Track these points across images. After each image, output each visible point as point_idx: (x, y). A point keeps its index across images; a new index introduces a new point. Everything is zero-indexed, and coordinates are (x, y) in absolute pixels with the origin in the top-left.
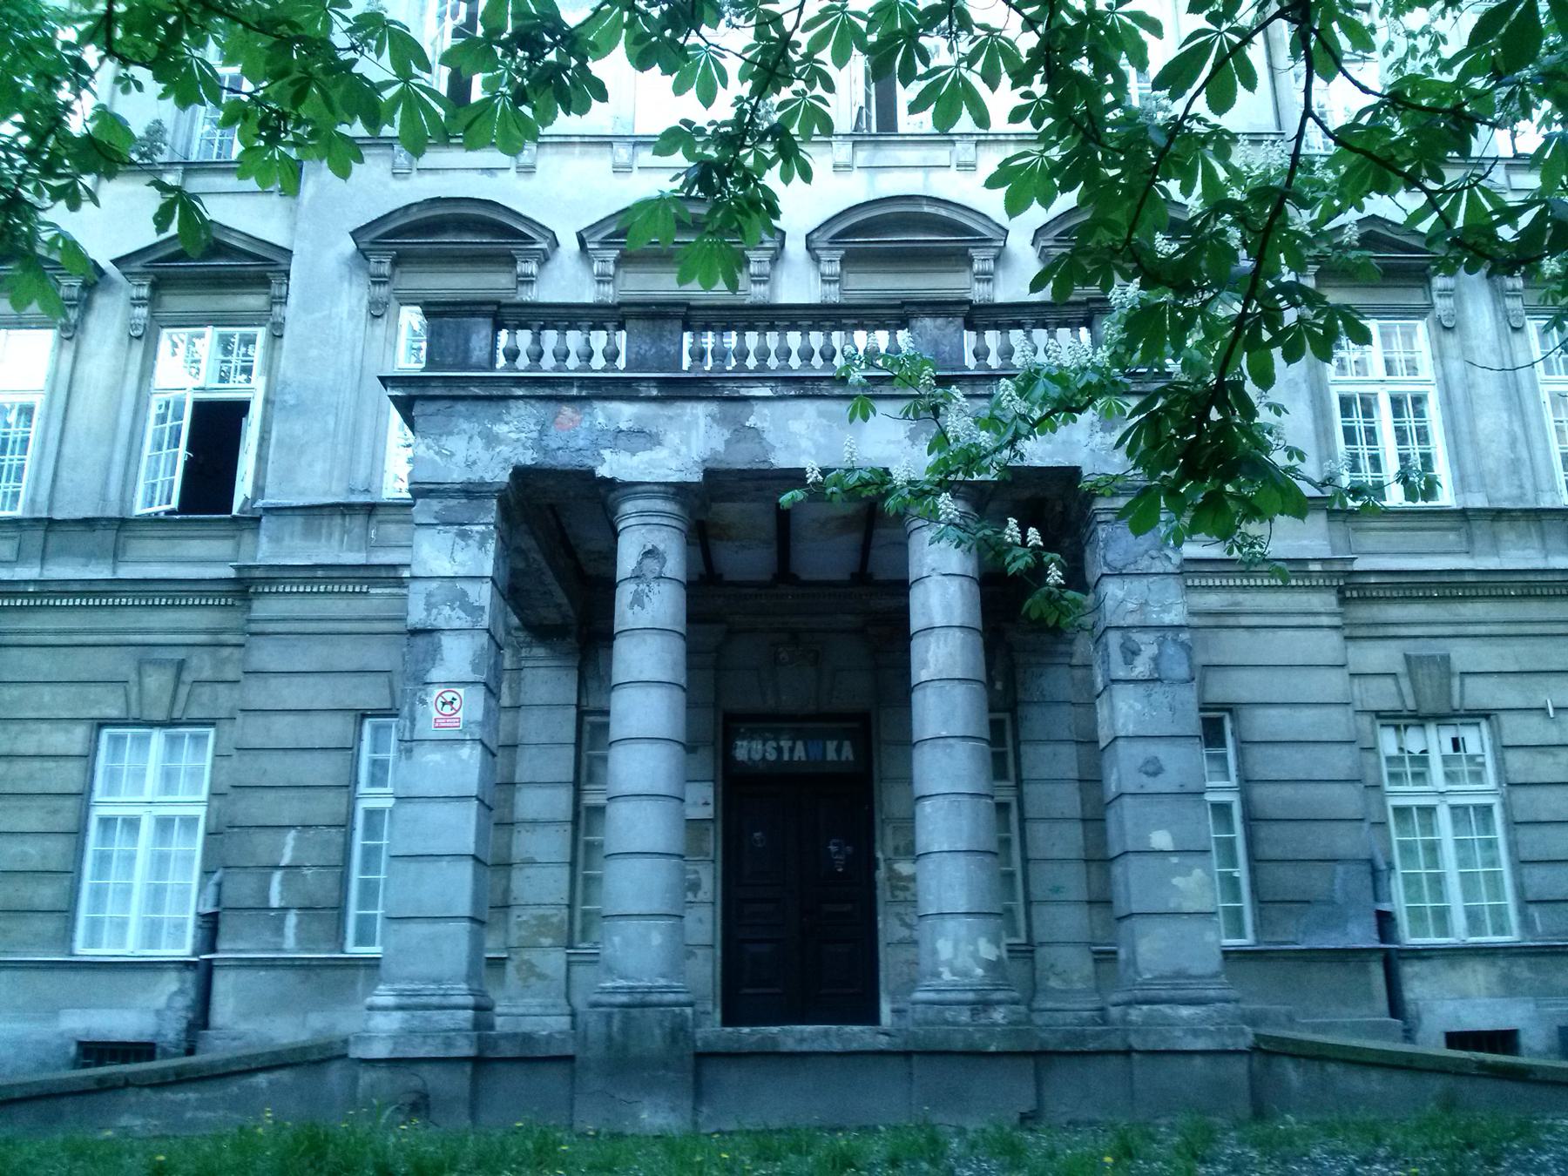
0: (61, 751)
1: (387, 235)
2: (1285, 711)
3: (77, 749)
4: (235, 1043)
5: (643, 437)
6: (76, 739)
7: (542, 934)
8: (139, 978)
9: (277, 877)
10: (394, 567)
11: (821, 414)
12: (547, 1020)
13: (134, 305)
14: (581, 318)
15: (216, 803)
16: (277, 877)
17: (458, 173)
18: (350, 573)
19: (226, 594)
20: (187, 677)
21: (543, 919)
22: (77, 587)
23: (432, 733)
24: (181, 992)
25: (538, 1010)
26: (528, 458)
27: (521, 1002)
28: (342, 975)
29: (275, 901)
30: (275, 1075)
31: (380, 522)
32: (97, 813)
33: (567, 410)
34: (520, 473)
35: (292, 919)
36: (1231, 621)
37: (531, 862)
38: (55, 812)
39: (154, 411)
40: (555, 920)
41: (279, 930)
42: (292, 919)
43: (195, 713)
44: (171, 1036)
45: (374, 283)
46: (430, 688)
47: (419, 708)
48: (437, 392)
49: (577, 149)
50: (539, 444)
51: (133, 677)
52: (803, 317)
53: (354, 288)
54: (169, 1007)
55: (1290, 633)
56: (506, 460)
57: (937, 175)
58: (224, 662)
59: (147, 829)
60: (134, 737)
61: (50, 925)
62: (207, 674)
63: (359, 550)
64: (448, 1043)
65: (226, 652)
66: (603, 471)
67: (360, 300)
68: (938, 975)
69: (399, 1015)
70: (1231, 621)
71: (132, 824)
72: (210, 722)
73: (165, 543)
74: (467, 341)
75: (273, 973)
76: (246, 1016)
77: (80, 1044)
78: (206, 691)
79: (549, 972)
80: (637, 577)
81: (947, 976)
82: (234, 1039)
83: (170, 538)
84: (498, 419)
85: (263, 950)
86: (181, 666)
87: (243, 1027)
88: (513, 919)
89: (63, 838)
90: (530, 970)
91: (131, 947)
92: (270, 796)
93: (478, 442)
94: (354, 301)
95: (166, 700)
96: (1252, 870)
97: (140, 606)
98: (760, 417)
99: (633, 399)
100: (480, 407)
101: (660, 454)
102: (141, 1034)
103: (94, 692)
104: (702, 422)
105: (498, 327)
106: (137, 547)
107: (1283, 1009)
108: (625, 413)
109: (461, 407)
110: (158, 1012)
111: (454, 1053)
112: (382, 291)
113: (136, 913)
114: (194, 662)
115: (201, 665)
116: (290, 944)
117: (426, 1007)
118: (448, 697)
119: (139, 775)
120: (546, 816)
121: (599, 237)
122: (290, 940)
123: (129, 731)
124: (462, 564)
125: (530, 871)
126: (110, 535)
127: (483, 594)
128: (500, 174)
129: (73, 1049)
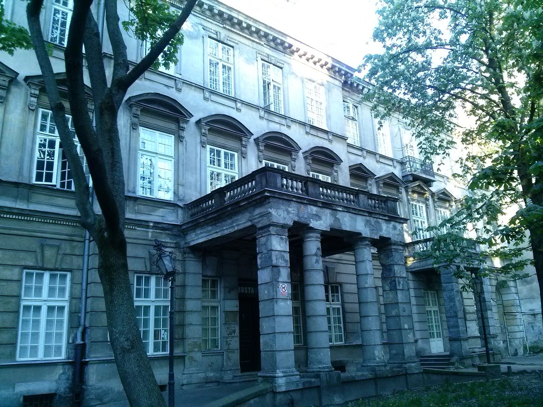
0: (9, 278)
1: (141, 101)
2: (350, 285)
3: (16, 278)
4: (99, 391)
5: (318, 217)
6: (14, 273)
7: (195, 348)
8: (46, 369)
10: (147, 222)
11: (350, 217)
12: (199, 374)
13: (32, 96)
14: (298, 178)
15: (74, 301)
17: (157, 84)
18: (133, 222)
20: (61, 252)
21: (195, 343)
22: (16, 211)
23: (281, 297)
24: (64, 373)
25: (196, 372)
26: (296, 219)
27: (190, 369)
30: (255, 399)
31: (138, 204)
32: (23, 303)
33: (302, 206)
34: (295, 222)
36: (340, 261)
37: (191, 324)
38: (8, 303)
39: (38, 142)
40: (198, 343)
43: (64, 266)
44: (62, 390)
45: (134, 116)
46: (279, 283)
47: (278, 289)
48: (277, 196)
49: (193, 88)
51: (38, 250)
52: (340, 189)
53: (125, 116)
54: (59, 379)
55: (350, 266)
56: (292, 219)
57: (282, 127)
58: (74, 247)
59: (44, 310)
60: (60, 275)
62: (68, 251)
63: (132, 213)
64: (297, 385)
65: (75, 243)
66: (311, 225)
67: (127, 121)
68: (376, 359)
69: (284, 378)
70: (340, 261)
71: (38, 309)
72: (70, 270)
73: (47, 197)
74: (276, 180)
75: (109, 365)
76: (100, 381)
78: (68, 258)
79: (198, 359)
81: (377, 359)
82: (98, 389)
83: (51, 196)
84: (289, 207)
85: (107, 357)
86: (59, 247)
87: (100, 385)
88: (187, 343)
89: (12, 314)
90: (192, 358)
93: (286, 212)
94: (126, 121)
95: (53, 261)
96: (344, 325)
97: (41, 222)
98: (340, 215)
100: (285, 202)
101: (321, 222)
102: (50, 390)
103: (22, 255)
104: (329, 215)
105: (282, 178)
106: (37, 197)
107: (351, 359)
109: (281, 201)
110: (56, 381)
111: (299, 388)
112: (136, 120)
113: (41, 343)
114: (63, 246)
115: (66, 248)
117: (290, 376)
118: (284, 286)
119: (39, 290)
120: (195, 309)
121: (205, 121)
123: (35, 271)
124: (282, 247)
125: (191, 327)
126: (25, 191)
127: (287, 256)
128: (171, 88)
129: (22, 399)
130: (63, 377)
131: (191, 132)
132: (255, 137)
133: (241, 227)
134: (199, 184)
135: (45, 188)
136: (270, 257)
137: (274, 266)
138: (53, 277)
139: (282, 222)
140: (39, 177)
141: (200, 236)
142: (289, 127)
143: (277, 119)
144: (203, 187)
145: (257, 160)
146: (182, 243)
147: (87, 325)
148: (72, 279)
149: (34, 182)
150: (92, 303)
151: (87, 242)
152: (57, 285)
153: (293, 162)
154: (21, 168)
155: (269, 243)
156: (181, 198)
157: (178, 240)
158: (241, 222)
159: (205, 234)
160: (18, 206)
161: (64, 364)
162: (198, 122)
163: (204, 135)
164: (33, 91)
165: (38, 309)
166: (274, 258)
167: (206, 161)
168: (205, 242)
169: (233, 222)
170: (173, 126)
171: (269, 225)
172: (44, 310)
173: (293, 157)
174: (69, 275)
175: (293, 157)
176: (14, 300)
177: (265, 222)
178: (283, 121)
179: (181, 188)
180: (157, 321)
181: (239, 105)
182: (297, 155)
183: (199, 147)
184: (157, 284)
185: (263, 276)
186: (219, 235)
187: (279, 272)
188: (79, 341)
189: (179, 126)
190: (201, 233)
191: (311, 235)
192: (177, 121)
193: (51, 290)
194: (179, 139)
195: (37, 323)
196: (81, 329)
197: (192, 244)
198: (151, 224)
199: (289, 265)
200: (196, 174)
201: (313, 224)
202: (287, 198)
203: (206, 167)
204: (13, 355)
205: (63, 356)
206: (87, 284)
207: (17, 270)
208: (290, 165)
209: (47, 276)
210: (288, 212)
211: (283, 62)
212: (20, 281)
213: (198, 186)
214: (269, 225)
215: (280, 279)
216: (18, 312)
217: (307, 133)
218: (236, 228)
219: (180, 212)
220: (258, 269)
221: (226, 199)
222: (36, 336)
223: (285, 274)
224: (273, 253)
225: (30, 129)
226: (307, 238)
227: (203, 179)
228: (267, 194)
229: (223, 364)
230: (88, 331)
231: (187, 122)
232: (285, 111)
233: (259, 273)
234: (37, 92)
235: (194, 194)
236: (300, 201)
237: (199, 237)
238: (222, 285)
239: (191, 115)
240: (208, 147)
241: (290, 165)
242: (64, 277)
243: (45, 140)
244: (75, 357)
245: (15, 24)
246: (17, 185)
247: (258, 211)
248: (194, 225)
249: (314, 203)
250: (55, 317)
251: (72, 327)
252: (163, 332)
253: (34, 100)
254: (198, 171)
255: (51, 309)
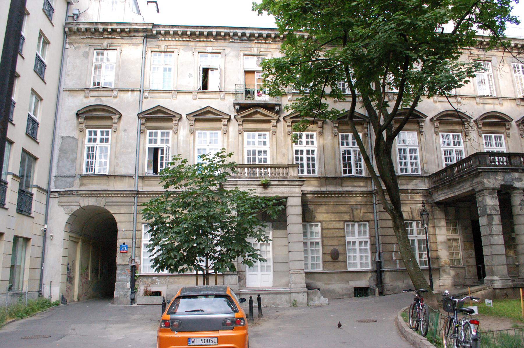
0: (338, 228)
3: (342, 227)
8: (363, 274)
9: (393, 253)
15: (372, 238)
16: (393, 253)
19: (367, 194)
24: (372, 277)
26: (503, 183)
28: (200, 262)
29: (394, 259)
32: (347, 240)
34: (502, 185)
35: (398, 262)
38: (339, 241)
39: (341, 152)
41: (396, 264)
42: (398, 262)
43: (365, 219)
50: (503, 180)
57: (496, 106)
61: (343, 264)
66: (514, 186)
71: (354, 243)
72: (368, 221)
77: (354, 288)
80: (520, 205)
84: (497, 176)
91: (358, 268)
92: (389, 237)
93: (494, 180)
99: (518, 172)
100: (493, 173)
106: (345, 183)
108: (516, 175)
109: (490, 173)
113: (358, 261)
116: (398, 267)
119: (353, 233)
122: (398, 266)
123: (350, 223)
126: (340, 181)
127: (498, 208)
130: (372, 279)
131: (427, 125)
132: (474, 119)
133: (466, 190)
134: (437, 160)
135: (349, 178)
136: (486, 209)
137: (488, 215)
138: (359, 225)
139: (492, 186)
140: (345, 172)
141: (441, 196)
142: (501, 104)
143: (490, 101)
144: (440, 164)
145: (477, 135)
146: (430, 200)
147: (381, 251)
148: (369, 226)
149: (343, 175)
150: (382, 239)
151: (375, 205)
152: (362, 230)
153: (507, 131)
154: (336, 169)
155: (484, 201)
156: (426, 171)
157: (428, 198)
158: (465, 188)
159: (444, 195)
160: (337, 190)
161: (371, 272)
162: (431, 120)
163: (436, 127)
164: (335, 125)
165: (354, 243)
166: (488, 210)
167: (440, 144)
168: (445, 199)
169: (460, 188)
170: (415, 126)
171: (483, 190)
172: (357, 244)
173: (507, 127)
174: (367, 224)
175: (507, 127)
176: (343, 239)
177: (479, 188)
178: (496, 101)
179: (425, 165)
180: (420, 249)
181: (459, 99)
182: (511, 125)
183: (434, 135)
184: (418, 226)
185: (483, 221)
186: (452, 195)
187: (492, 218)
188: (378, 260)
189: (419, 125)
190: (441, 194)
191: (516, 191)
192: (418, 123)
193: (360, 233)
194: (420, 133)
195: (354, 250)
196: (377, 253)
197: (436, 200)
198: (410, 191)
199: (499, 213)
200: (434, 154)
201: (517, 184)
202: (495, 171)
203: (440, 148)
204: (346, 267)
205: (370, 268)
206: (378, 228)
207: (342, 223)
208: (505, 134)
209: (356, 225)
210: (496, 180)
211: (490, 56)
212: (344, 229)
213: (437, 162)
214: (483, 190)
215: (494, 223)
216: (345, 245)
217: (518, 105)
218: (463, 191)
219: (426, 180)
220: (478, 217)
221: (455, 172)
222: (355, 257)
223: (497, 219)
224: (487, 207)
225: (337, 146)
226: (515, 193)
227: (439, 156)
228: (479, 170)
229: (465, 275)
230: (382, 254)
231: (424, 121)
232: (497, 93)
233: (480, 219)
234: (337, 125)
235: (434, 167)
236: (505, 171)
237: (440, 197)
238: (460, 225)
239: (426, 117)
240: (440, 134)
241: (505, 134)
242: (365, 225)
243: (345, 151)
244: (377, 269)
245: (276, 19)
246: (335, 178)
247: (475, 181)
248: (435, 189)
249: (516, 171)
250: (363, 247)
251: (373, 252)
252: (424, 255)
253: (336, 129)
254: (435, 152)
255: (361, 243)
